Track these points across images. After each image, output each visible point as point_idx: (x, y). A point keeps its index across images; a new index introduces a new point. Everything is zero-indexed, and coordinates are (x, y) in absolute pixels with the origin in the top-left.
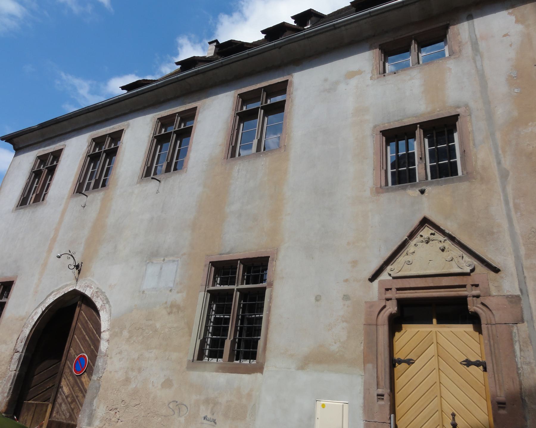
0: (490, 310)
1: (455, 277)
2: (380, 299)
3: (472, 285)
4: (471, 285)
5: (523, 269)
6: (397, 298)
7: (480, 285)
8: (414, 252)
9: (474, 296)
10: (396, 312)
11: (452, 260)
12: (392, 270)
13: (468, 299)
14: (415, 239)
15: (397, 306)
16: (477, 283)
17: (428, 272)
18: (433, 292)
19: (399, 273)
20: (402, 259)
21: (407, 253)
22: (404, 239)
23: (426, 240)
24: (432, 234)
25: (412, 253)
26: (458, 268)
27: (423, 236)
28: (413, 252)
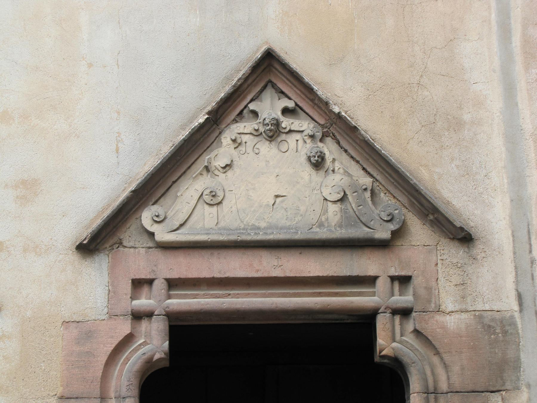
2: (112, 316)
5: (530, 238)
7: (414, 278)
9: (395, 312)
15: (168, 338)
18: (279, 297)
24: (286, 111)
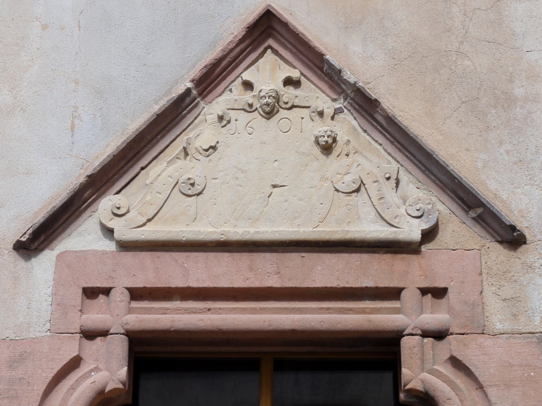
0: (481, 387)
1: (365, 257)
3: (424, 291)
4: (419, 288)
6: (128, 327)
8: (214, 148)
9: (425, 334)
10: (121, 386)
11: (358, 190)
12: (119, 212)
13: (405, 342)
14: (220, 95)
16: (440, 284)
17: (262, 229)
19: (149, 227)
20: (163, 171)
21: (185, 149)
22: (180, 90)
23: (268, 105)
24: (289, 82)
25: (207, 150)
26: (380, 220)
27: (257, 87)
28: (211, 147)
